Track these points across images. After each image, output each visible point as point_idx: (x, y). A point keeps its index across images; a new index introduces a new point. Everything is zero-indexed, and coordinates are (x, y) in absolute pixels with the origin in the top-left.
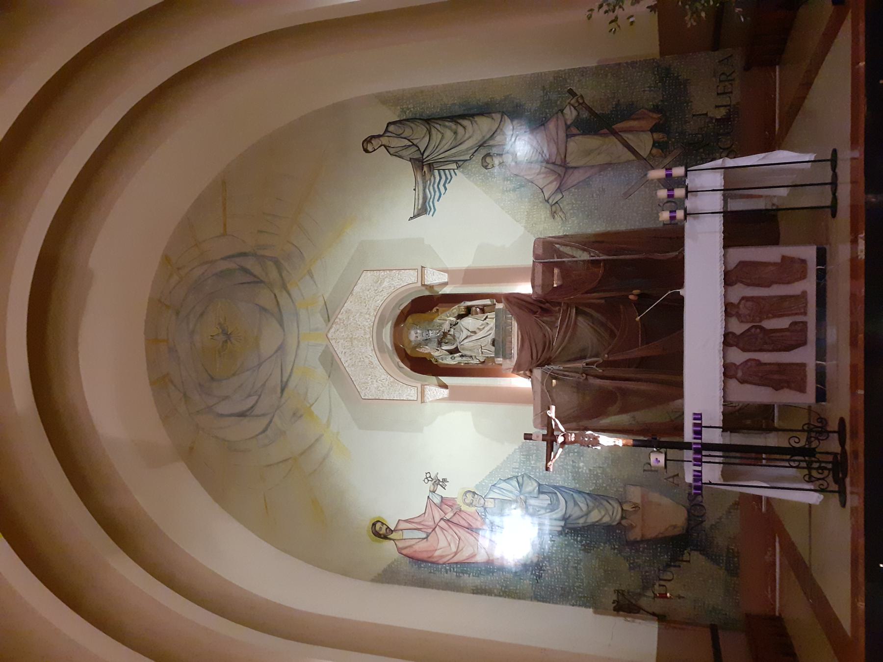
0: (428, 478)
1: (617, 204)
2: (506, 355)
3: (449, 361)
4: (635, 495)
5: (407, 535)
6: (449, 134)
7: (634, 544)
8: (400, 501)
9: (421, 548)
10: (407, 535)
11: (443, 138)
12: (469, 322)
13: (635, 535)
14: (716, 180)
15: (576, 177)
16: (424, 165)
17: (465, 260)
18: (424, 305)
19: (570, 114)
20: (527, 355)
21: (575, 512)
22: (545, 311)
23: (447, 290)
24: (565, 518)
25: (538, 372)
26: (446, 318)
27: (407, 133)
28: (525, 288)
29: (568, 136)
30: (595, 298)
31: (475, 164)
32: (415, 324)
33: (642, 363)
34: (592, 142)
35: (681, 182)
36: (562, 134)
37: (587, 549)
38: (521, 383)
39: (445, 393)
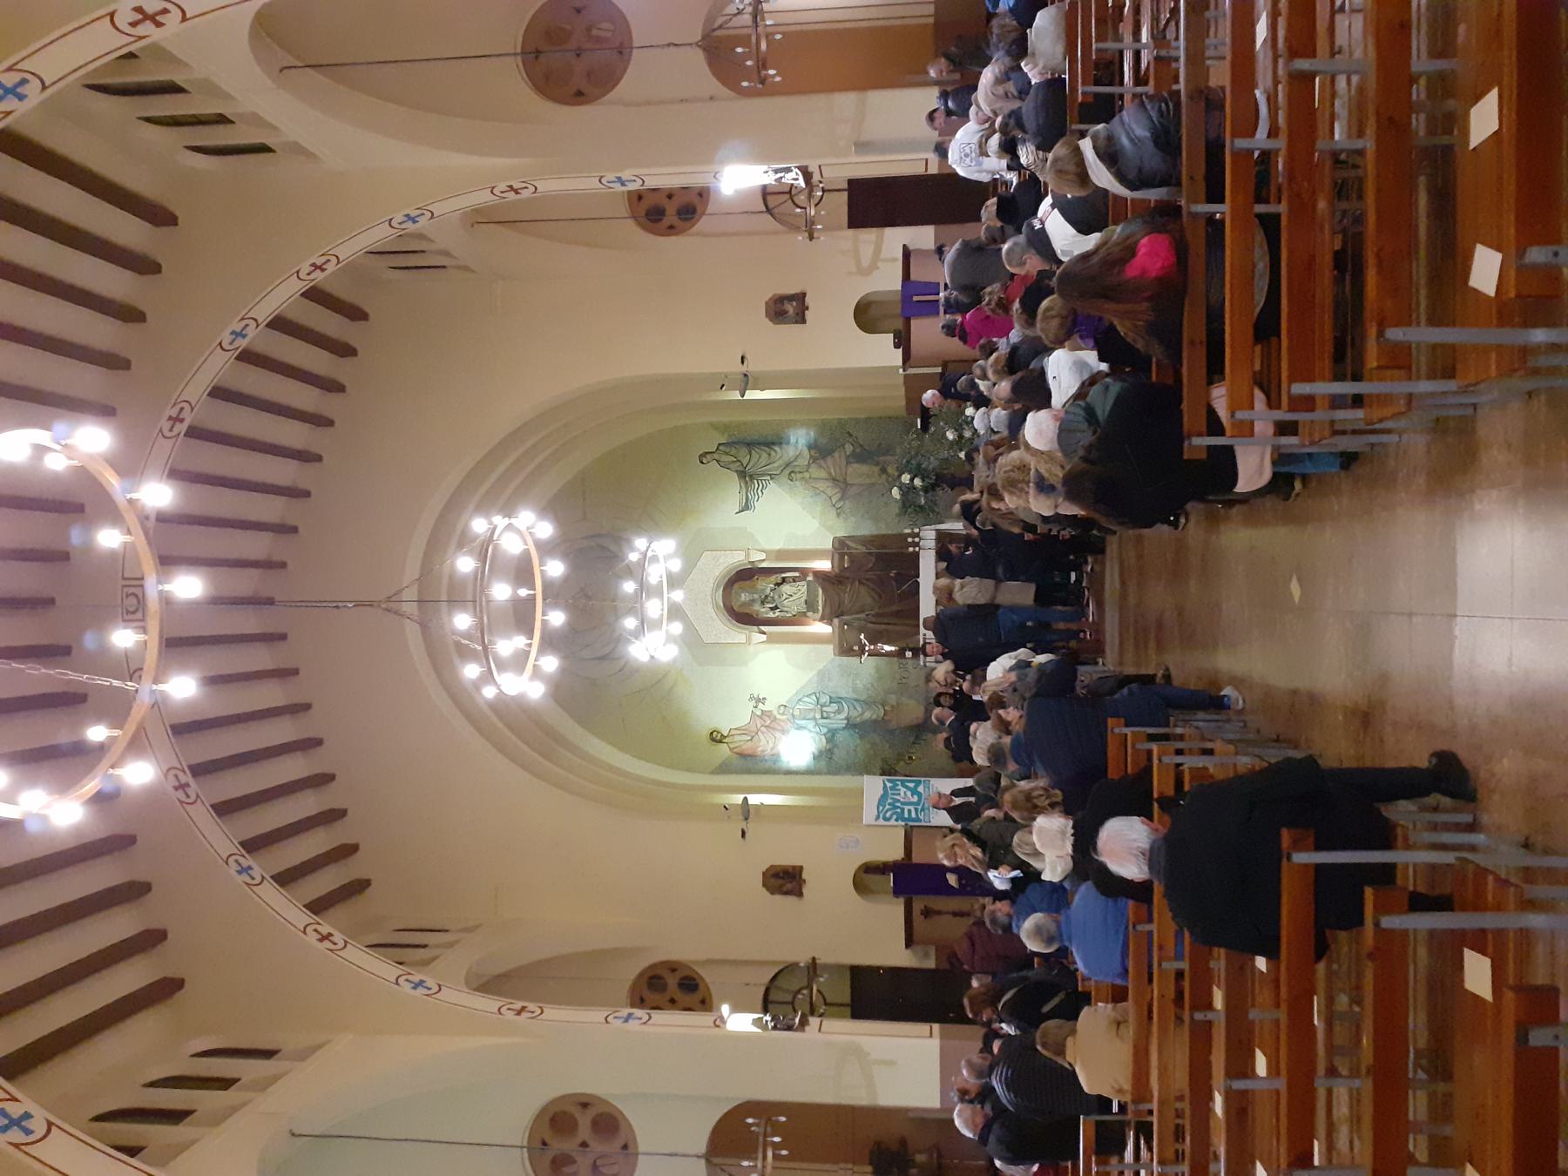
0: (751, 698)
1: (887, 523)
2: (815, 611)
3: (771, 615)
4: (892, 699)
5: (737, 738)
6: (765, 455)
7: (892, 732)
8: (731, 716)
9: (746, 747)
10: (737, 738)
11: (759, 458)
12: (786, 588)
13: (893, 725)
14: (932, 535)
15: (853, 491)
16: (747, 476)
17: (778, 544)
18: (745, 575)
19: (849, 448)
20: (828, 610)
21: (854, 714)
22: (840, 582)
23: (764, 565)
24: (847, 719)
25: (836, 621)
26: (766, 585)
27: (733, 452)
28: (825, 565)
29: (848, 463)
30: (870, 575)
31: (784, 479)
32: (743, 589)
33: (898, 614)
34: (864, 468)
35: (917, 535)
36: (844, 462)
37: (861, 737)
38: (824, 629)
39: (764, 637)
